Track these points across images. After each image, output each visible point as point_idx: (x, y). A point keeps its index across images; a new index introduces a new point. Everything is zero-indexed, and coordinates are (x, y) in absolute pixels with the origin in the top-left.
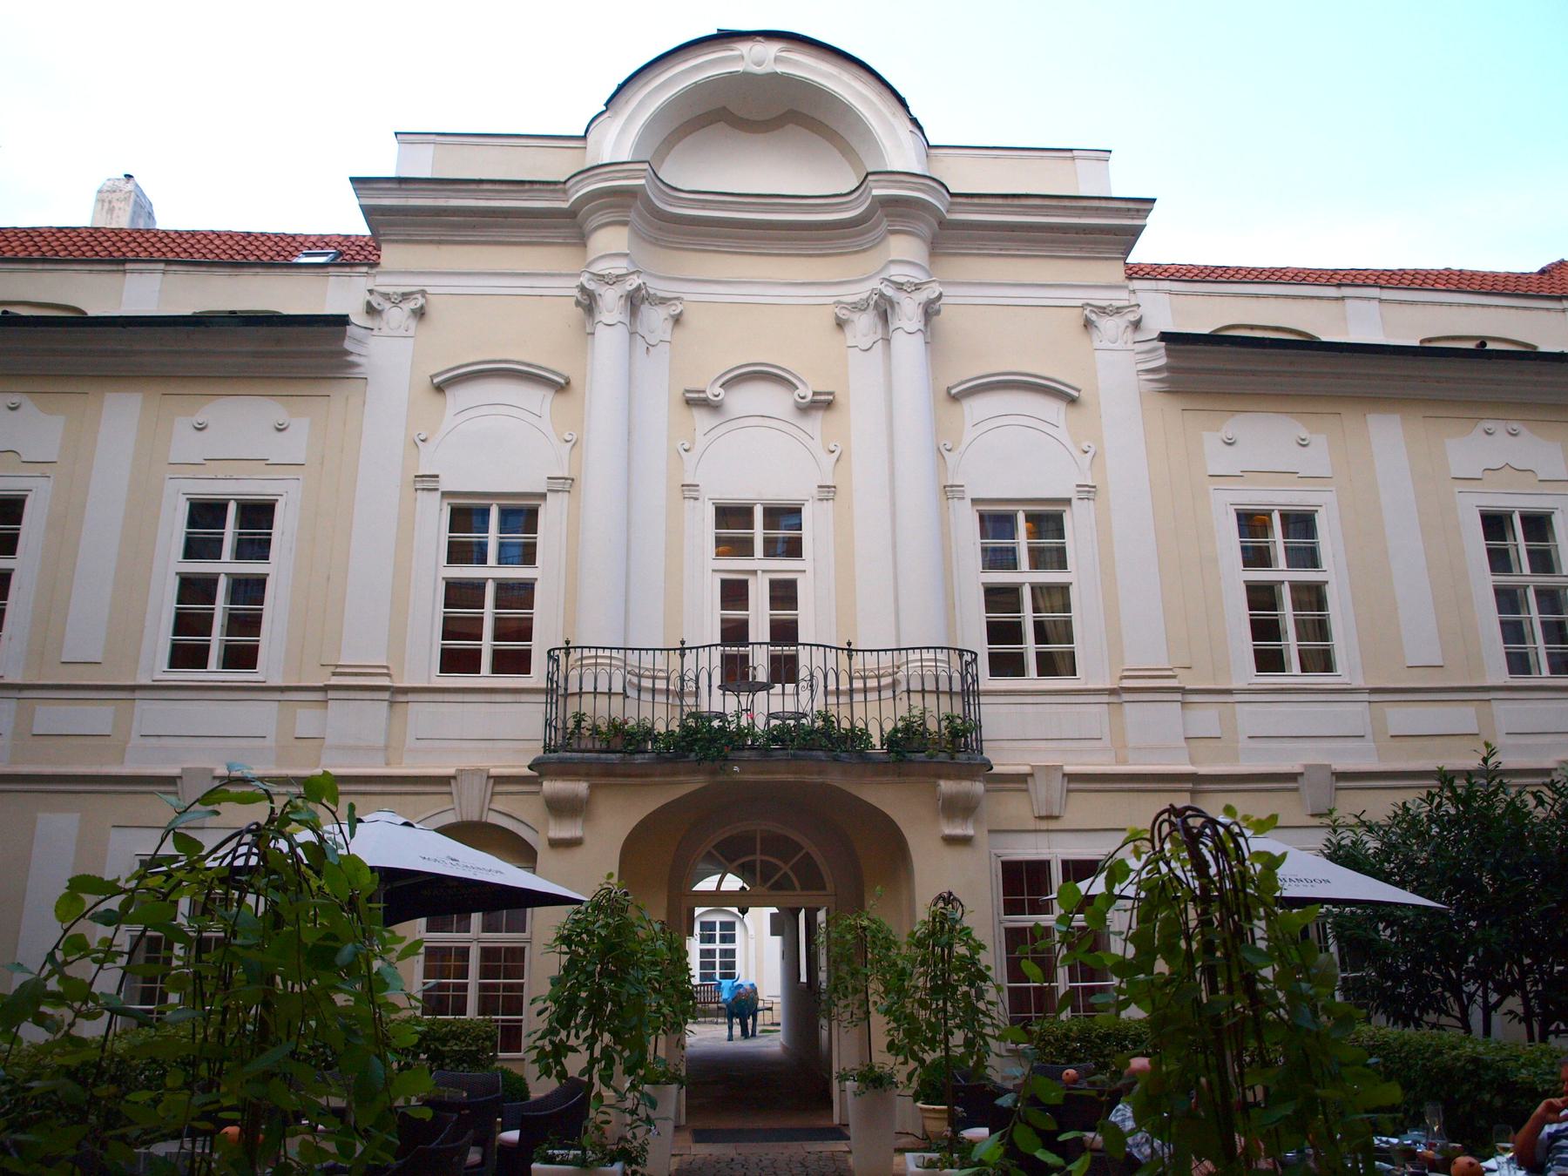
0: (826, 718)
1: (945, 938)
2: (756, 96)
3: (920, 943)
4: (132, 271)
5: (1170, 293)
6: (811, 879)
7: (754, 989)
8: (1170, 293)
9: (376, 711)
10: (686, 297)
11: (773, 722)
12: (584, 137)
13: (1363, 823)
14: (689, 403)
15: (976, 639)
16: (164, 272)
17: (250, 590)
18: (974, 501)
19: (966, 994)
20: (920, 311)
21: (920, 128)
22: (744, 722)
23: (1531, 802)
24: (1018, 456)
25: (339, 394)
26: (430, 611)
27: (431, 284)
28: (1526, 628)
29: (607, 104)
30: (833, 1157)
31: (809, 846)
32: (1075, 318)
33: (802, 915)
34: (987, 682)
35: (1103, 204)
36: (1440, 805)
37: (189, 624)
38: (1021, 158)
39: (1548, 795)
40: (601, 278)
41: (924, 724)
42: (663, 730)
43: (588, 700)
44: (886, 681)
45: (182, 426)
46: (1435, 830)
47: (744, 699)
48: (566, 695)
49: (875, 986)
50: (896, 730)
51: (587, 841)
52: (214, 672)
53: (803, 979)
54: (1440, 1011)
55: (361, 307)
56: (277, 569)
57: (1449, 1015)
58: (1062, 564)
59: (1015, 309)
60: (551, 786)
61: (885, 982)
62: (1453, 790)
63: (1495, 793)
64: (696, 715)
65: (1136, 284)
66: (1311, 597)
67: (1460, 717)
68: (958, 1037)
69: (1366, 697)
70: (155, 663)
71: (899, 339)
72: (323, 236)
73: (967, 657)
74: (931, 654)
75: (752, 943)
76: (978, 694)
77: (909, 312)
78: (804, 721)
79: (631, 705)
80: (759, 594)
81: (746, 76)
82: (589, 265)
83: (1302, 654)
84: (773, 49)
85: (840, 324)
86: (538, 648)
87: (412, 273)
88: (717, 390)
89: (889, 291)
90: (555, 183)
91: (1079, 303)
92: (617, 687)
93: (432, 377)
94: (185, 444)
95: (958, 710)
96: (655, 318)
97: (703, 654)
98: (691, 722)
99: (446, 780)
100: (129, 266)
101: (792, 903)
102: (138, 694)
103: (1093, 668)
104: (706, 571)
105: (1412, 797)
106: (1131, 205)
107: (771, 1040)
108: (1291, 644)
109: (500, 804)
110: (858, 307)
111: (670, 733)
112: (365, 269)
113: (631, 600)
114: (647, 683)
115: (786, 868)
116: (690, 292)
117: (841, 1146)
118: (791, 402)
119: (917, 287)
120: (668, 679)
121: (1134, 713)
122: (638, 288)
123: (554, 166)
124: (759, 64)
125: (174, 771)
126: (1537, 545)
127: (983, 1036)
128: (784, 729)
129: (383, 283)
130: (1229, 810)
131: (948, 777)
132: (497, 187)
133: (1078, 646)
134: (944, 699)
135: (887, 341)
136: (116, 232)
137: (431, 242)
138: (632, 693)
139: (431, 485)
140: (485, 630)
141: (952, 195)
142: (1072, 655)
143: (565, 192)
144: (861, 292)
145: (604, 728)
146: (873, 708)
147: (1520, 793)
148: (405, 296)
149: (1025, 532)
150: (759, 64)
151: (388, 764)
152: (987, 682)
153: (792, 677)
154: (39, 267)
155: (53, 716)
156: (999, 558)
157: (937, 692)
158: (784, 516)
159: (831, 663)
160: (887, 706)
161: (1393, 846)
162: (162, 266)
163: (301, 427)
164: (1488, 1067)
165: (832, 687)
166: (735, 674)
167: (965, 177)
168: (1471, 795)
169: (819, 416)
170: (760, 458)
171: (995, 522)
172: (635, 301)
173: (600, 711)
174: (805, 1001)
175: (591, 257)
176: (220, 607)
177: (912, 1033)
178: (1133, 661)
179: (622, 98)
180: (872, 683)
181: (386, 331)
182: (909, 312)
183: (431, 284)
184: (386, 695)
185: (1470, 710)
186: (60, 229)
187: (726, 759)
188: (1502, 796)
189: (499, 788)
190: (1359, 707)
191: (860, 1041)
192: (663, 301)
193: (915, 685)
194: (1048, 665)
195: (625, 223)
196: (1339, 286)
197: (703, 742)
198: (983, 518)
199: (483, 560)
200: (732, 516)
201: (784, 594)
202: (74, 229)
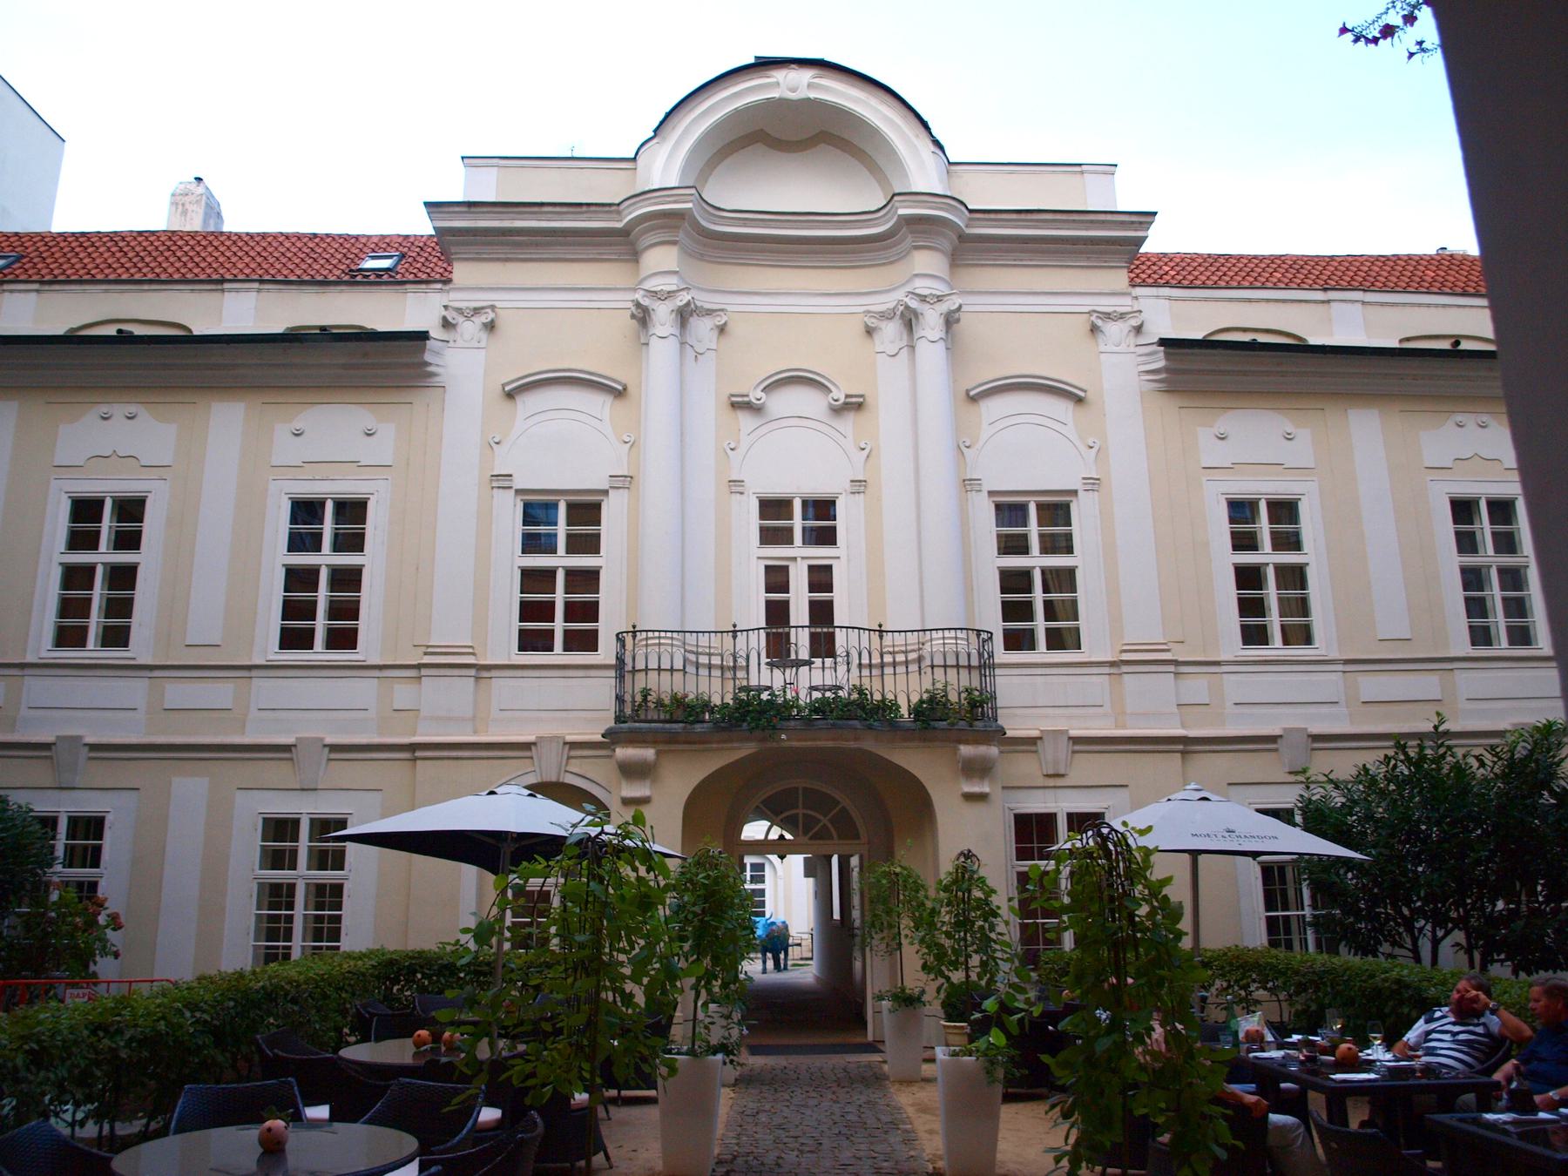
0: (861, 692)
1: (965, 886)
2: (791, 117)
3: (946, 889)
4: (230, 290)
5: (1169, 298)
6: (846, 829)
7: (786, 927)
8: (1169, 298)
9: (464, 685)
10: (729, 308)
11: (817, 695)
12: (634, 159)
13: (1331, 781)
14: (734, 406)
15: (993, 622)
16: (259, 291)
17: (348, 579)
18: (991, 493)
19: (982, 927)
20: (941, 321)
21: (941, 148)
22: (789, 697)
23: (1475, 764)
24: (1030, 450)
25: (419, 399)
26: (509, 596)
27: (501, 299)
28: (1489, 604)
29: (655, 131)
30: (869, 1065)
31: (845, 801)
32: (1082, 323)
33: (835, 860)
34: (1001, 655)
35: (1109, 217)
36: (1395, 766)
37: (296, 610)
38: (1034, 173)
39: (1488, 758)
40: (654, 294)
41: (946, 696)
42: (718, 702)
43: (653, 675)
44: (912, 656)
45: (282, 432)
46: (1392, 787)
47: (790, 673)
48: (634, 671)
49: (906, 923)
50: (921, 701)
51: (655, 799)
52: (319, 653)
53: (836, 916)
54: (1394, 944)
55: (437, 321)
56: (372, 560)
57: (1402, 946)
58: (1069, 550)
59: (1026, 317)
60: (624, 753)
61: (913, 918)
62: (1406, 754)
63: (1443, 756)
64: (747, 689)
65: (1139, 291)
66: (1294, 577)
67: (1425, 685)
68: (975, 960)
69: (1340, 667)
70: (267, 647)
71: (922, 347)
72: (384, 237)
73: (984, 636)
74: (953, 633)
75: (781, 883)
76: (993, 666)
77: (932, 320)
78: (841, 693)
79: (691, 679)
80: (799, 580)
81: (782, 102)
82: (641, 282)
83: (1284, 629)
84: (806, 75)
85: (870, 332)
86: (607, 626)
87: (482, 289)
88: (759, 394)
89: (914, 304)
90: (610, 205)
91: (1086, 309)
92: (678, 664)
93: (503, 386)
94: (286, 449)
95: (976, 683)
96: (702, 328)
97: (753, 636)
98: (743, 696)
99: (527, 746)
100: (226, 286)
101: (824, 851)
102: (254, 673)
103: (1096, 642)
104: (752, 559)
105: (1371, 758)
106: (1134, 218)
107: (804, 971)
108: (1274, 620)
109: (575, 766)
110: (886, 316)
111: (725, 706)
112: (439, 286)
113: (686, 588)
114: (704, 660)
115: (825, 821)
116: (733, 303)
117: (876, 1057)
118: (825, 404)
119: (940, 299)
120: (722, 656)
121: (1132, 682)
122: (688, 304)
123: (607, 188)
124: (793, 90)
125: (290, 740)
126: (1501, 528)
127: (994, 959)
128: (824, 700)
129: (457, 298)
130: (1125, 824)
131: (967, 742)
132: (558, 209)
133: (1082, 623)
134: (964, 673)
135: (912, 347)
136: (193, 235)
137: (498, 260)
138: (691, 669)
139: (506, 484)
140: (557, 611)
141: (971, 211)
142: (1077, 630)
143: (619, 213)
144: (887, 302)
145: (667, 701)
146: (901, 678)
147: (1465, 756)
148: (477, 311)
149: (1034, 522)
150: (793, 90)
151: (475, 732)
152: (1001, 655)
153: (831, 653)
154: (146, 287)
155: (180, 693)
156: (1012, 545)
157: (958, 666)
158: (822, 508)
159: (865, 643)
160: (914, 677)
161: (1355, 802)
162: (256, 285)
163: (387, 432)
164: (1407, 986)
165: (865, 661)
166: (778, 650)
167: (984, 194)
168: (1422, 758)
169: (851, 417)
170: (797, 457)
171: (1010, 511)
172: (684, 315)
173: (664, 686)
174: (838, 937)
175: (643, 274)
176: (323, 595)
177: (941, 955)
178: (1133, 636)
179: (670, 123)
180: (900, 658)
181: (460, 343)
182: (932, 320)
183: (501, 299)
184: (472, 672)
185: (1434, 679)
186: (140, 233)
187: (774, 728)
188: (1449, 759)
189: (573, 753)
190: (1333, 677)
191: (899, 966)
192: (710, 312)
193: (938, 661)
194: (1057, 640)
195: (674, 243)
196: (1325, 290)
197: (754, 714)
198: (999, 507)
199: (553, 551)
200: (773, 507)
201: (821, 578)
202: (153, 233)
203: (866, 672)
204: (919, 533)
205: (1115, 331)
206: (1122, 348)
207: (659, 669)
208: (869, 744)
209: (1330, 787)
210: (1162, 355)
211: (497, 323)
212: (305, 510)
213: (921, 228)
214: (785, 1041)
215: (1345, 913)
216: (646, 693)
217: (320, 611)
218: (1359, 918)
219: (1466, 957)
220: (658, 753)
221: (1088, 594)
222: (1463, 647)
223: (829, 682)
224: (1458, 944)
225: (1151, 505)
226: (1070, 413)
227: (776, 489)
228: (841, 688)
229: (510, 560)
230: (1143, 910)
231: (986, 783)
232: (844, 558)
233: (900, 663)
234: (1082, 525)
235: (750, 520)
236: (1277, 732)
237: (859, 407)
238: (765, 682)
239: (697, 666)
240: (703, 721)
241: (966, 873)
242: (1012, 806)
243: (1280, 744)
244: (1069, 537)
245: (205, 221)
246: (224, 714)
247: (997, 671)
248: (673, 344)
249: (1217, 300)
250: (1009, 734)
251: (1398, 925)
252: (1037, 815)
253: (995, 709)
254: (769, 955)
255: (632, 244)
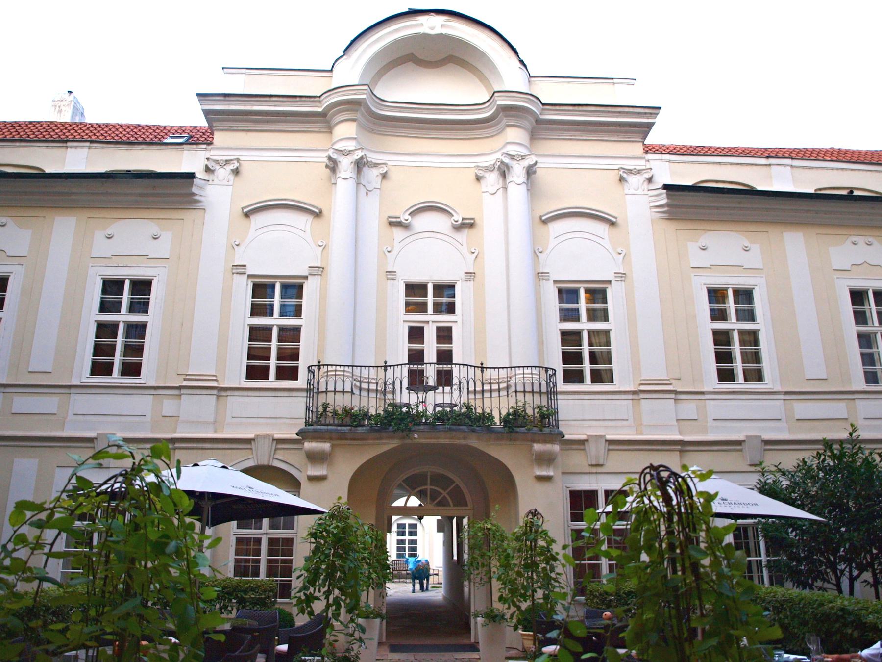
0: (468, 407)
1: (532, 536)
3: (518, 539)
4: (71, 147)
5: (669, 161)
6: (460, 500)
7: (427, 563)
8: (669, 161)
9: (210, 401)
10: (389, 163)
11: (438, 409)
13: (780, 470)
14: (391, 224)
15: (558, 365)
16: (89, 147)
17: (137, 330)
18: (555, 282)
19: (544, 569)
24: (580, 255)
25: (189, 216)
26: (241, 344)
27: (243, 155)
29: (344, 52)
31: (458, 481)
32: (615, 176)
33: (455, 521)
34: (561, 386)
35: (631, 110)
36: (824, 460)
40: (340, 152)
41: (525, 411)
42: (374, 413)
43: (331, 396)
44: (503, 386)
45: (99, 236)
46: (821, 474)
50: (508, 414)
51: (330, 477)
52: (116, 378)
53: (455, 558)
54: (824, 580)
55: (202, 168)
57: (829, 582)
58: (606, 319)
59: (578, 170)
60: (308, 445)
62: (832, 451)
64: (393, 405)
65: (649, 156)
66: (751, 338)
67: (838, 409)
68: (540, 594)
69: (782, 397)
70: (83, 374)
71: (511, 188)
72: (181, 127)
73: (550, 372)
76: (556, 393)
77: (518, 172)
78: (455, 408)
80: (430, 335)
81: (425, 36)
84: (442, 19)
85: (478, 179)
88: (407, 216)
89: (506, 160)
91: (617, 167)
93: (243, 209)
94: (101, 247)
95: (545, 403)
96: (372, 175)
97: (398, 369)
98: (390, 409)
100: (69, 144)
102: (72, 390)
104: (400, 322)
106: (647, 111)
107: (437, 594)
108: (738, 366)
111: (378, 415)
112: (204, 146)
113: (355, 339)
114: (365, 386)
115: (445, 494)
117: (475, 655)
118: (449, 224)
119: (523, 158)
120: (377, 383)
121: (646, 405)
122: (362, 158)
124: (432, 29)
128: (444, 413)
131: (538, 442)
132: (281, 99)
134: (537, 397)
135: (505, 188)
136: (63, 124)
137: (243, 130)
138: (356, 391)
139: (242, 271)
140: (272, 355)
141: (544, 105)
143: (320, 102)
144: (490, 160)
145: (340, 412)
146: (495, 401)
147: (871, 454)
148: (227, 162)
151: (215, 432)
152: (561, 386)
154: (18, 144)
157: (533, 392)
158: (445, 289)
159: (471, 375)
160: (504, 400)
161: (797, 484)
162: (88, 144)
164: (850, 613)
165: (472, 389)
166: (416, 381)
167: (550, 93)
168: (842, 454)
170: (431, 257)
171: (567, 294)
172: (360, 165)
173: (338, 402)
174: (456, 570)
178: (647, 374)
179: (352, 49)
180: (495, 387)
181: (216, 182)
182: (518, 172)
183: (243, 155)
184: (215, 392)
185: (843, 405)
186: (31, 123)
187: (410, 430)
188: (860, 455)
189: (280, 446)
190: (778, 403)
192: (376, 165)
194: (597, 377)
195: (354, 120)
197: (397, 420)
198: (560, 291)
200: (415, 289)
201: (444, 335)
203: (472, 396)
204: (508, 306)
205: (634, 181)
206: (640, 192)
207: (335, 391)
208: (474, 442)
209: (778, 475)
210: (665, 195)
211: (240, 169)
212: (112, 286)
213: (511, 113)
214: (411, 642)
215: (791, 559)
216: (326, 406)
217: (117, 351)
218: (799, 561)
219: (873, 589)
220: (332, 446)
221: (618, 349)
222: (860, 384)
223: (447, 400)
224: (865, 581)
225: (658, 285)
226: (606, 232)
227: (417, 277)
228: (456, 405)
229: (243, 320)
230: (706, 562)
231: (551, 469)
232: (458, 322)
233: (495, 390)
234: (614, 302)
235: (400, 297)
236: (741, 438)
237: (471, 225)
238: (405, 400)
239: (361, 389)
240: (364, 426)
241: (533, 528)
242: (568, 485)
243: (745, 447)
244: (605, 311)
245: (74, 114)
246: (53, 417)
247: (559, 397)
248: (351, 183)
249: (699, 163)
250: (567, 437)
251: (827, 568)
252: (585, 491)
253: (557, 421)
254: (417, 581)
255: (328, 122)
